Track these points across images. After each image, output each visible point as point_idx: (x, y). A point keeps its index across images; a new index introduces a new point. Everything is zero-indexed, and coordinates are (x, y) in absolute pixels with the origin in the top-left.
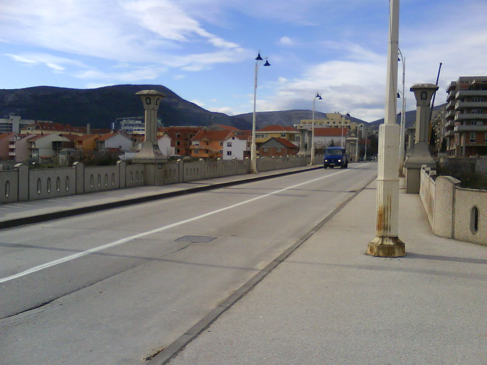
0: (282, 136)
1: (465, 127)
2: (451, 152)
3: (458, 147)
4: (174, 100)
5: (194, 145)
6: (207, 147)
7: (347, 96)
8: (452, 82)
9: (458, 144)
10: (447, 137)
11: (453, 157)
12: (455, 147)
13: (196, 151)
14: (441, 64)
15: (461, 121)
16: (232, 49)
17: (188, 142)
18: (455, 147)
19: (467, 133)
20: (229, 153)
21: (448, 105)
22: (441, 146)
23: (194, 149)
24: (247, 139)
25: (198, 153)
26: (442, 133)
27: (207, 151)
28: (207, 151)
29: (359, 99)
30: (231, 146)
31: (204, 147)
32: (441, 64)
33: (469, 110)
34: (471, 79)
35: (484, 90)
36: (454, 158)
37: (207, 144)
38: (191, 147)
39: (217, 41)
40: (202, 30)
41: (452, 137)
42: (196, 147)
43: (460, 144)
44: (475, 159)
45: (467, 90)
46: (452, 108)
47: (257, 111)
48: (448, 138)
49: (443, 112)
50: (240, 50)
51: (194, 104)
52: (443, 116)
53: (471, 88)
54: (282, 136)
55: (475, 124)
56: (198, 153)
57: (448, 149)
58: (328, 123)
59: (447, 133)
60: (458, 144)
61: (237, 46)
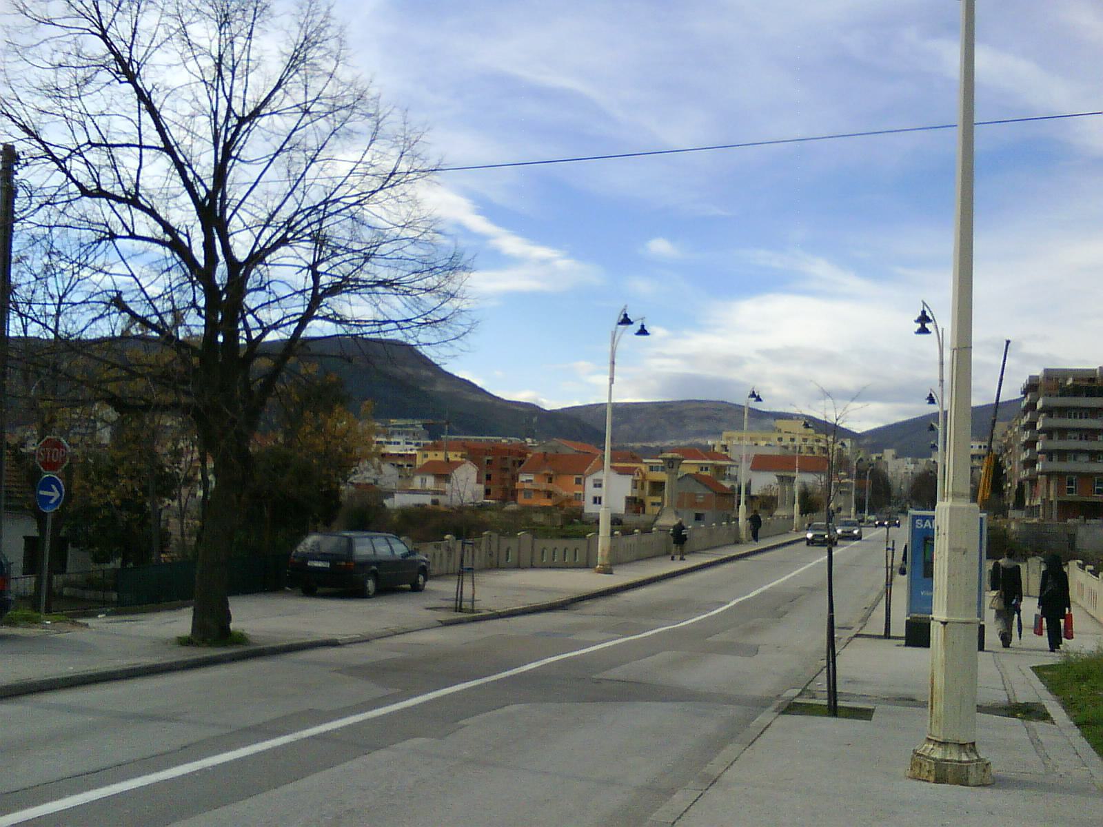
0: (702, 469)
1: (1056, 466)
2: (1033, 511)
3: (1043, 501)
4: (425, 373)
5: (523, 482)
6: (551, 487)
7: (795, 370)
8: (1030, 377)
9: (1045, 497)
10: (1026, 479)
11: (1035, 520)
12: (1038, 502)
13: (528, 493)
14: (1008, 342)
15: (1049, 454)
16: (544, 262)
17: (508, 476)
18: (1038, 502)
19: (1060, 475)
20: (597, 500)
21: (1026, 401)
22: (1013, 495)
23: (522, 490)
24: (633, 474)
25: (530, 497)
26: (1016, 471)
27: (549, 494)
28: (549, 494)
29: (828, 378)
30: (600, 486)
31: (544, 486)
32: (1008, 342)
33: (1063, 432)
34: (1065, 373)
35: (1091, 396)
36: (1036, 523)
37: (550, 481)
38: (518, 486)
39: (511, 244)
40: (480, 217)
41: (1033, 481)
42: (527, 486)
43: (1048, 496)
44: (1076, 526)
45: (1057, 396)
46: (1031, 406)
47: (616, 400)
48: (1028, 482)
49: (1016, 430)
50: (565, 265)
51: (468, 382)
52: (1017, 438)
53: (1065, 392)
54: (702, 469)
55: (1075, 459)
56: (530, 497)
57: (1027, 503)
58: (780, 439)
59: (1024, 474)
60: (1045, 497)
61: (556, 255)
